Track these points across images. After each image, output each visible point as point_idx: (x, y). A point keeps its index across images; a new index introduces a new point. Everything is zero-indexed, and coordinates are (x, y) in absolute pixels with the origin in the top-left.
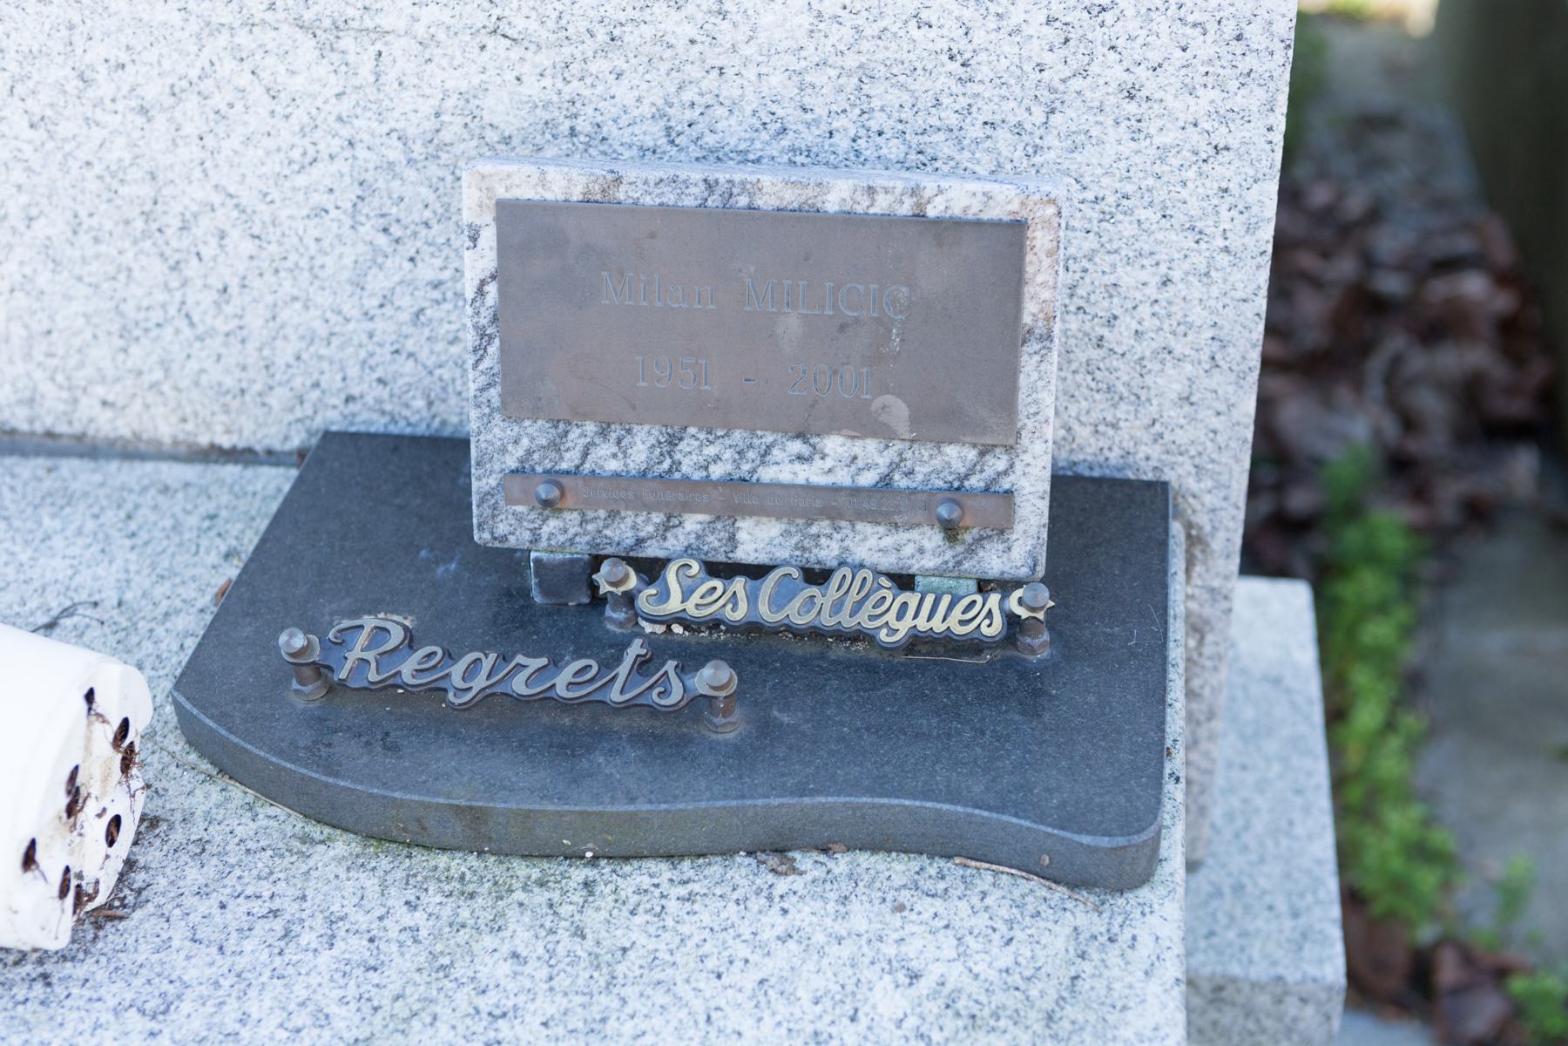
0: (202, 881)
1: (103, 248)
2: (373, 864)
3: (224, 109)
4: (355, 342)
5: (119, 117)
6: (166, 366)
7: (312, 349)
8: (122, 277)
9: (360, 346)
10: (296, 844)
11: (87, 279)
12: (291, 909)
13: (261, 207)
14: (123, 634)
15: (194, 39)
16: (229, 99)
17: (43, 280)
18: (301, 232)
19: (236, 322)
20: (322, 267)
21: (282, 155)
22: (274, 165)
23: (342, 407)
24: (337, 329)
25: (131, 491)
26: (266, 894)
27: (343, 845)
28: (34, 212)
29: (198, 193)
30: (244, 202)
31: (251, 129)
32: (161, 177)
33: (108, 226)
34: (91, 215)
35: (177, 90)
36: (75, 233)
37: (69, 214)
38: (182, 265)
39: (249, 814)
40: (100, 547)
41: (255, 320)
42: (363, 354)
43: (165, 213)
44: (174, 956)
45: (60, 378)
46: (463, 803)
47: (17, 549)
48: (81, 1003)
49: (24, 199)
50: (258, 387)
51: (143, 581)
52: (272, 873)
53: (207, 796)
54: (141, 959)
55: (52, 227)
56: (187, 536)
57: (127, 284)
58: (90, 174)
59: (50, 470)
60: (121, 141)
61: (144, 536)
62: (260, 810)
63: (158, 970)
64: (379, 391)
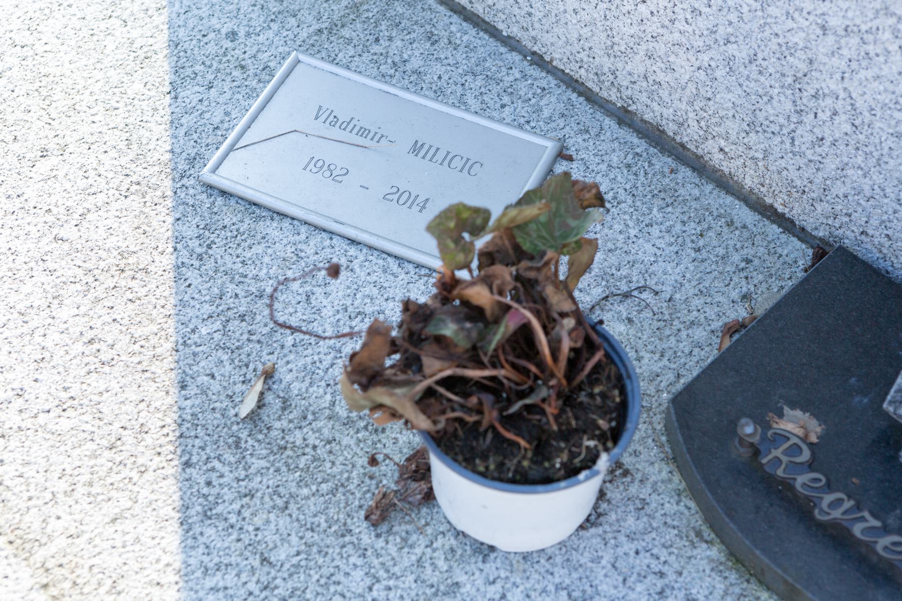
0: (633, 529)
1: (762, 79)
2: (727, 574)
3: (872, 54)
4: (884, 209)
5: (807, 23)
6: (766, 153)
7: (856, 197)
8: (765, 99)
9: (886, 213)
10: (692, 534)
11: (745, 88)
12: (672, 576)
13: (866, 114)
14: (663, 324)
15: (874, 11)
16: (878, 51)
17: (719, 73)
18: (883, 139)
19: (820, 158)
20: (887, 163)
21: (893, 97)
22: (886, 98)
23: (857, 234)
24: (877, 197)
25: (711, 213)
26: (663, 559)
27: (715, 552)
28: (732, 39)
29: (833, 85)
30: (858, 105)
31: (883, 73)
32: (815, 65)
33: (771, 70)
34: (764, 59)
35: (849, 29)
36: (750, 62)
37: (752, 52)
38: (804, 114)
39: (676, 498)
40: (676, 249)
41: (831, 165)
42: (885, 217)
43: (808, 83)
44: (600, 570)
45: (703, 124)
46: (790, 580)
47: (631, 224)
48: (542, 570)
49: (730, 30)
50: (814, 195)
51: (689, 289)
52: (671, 546)
53: (660, 472)
54: (583, 561)
55: (741, 52)
56: (728, 269)
57: (766, 103)
58: (775, 40)
59: (672, 171)
60: (802, 35)
61: (704, 254)
62: (684, 499)
63: (588, 573)
64: (884, 240)
